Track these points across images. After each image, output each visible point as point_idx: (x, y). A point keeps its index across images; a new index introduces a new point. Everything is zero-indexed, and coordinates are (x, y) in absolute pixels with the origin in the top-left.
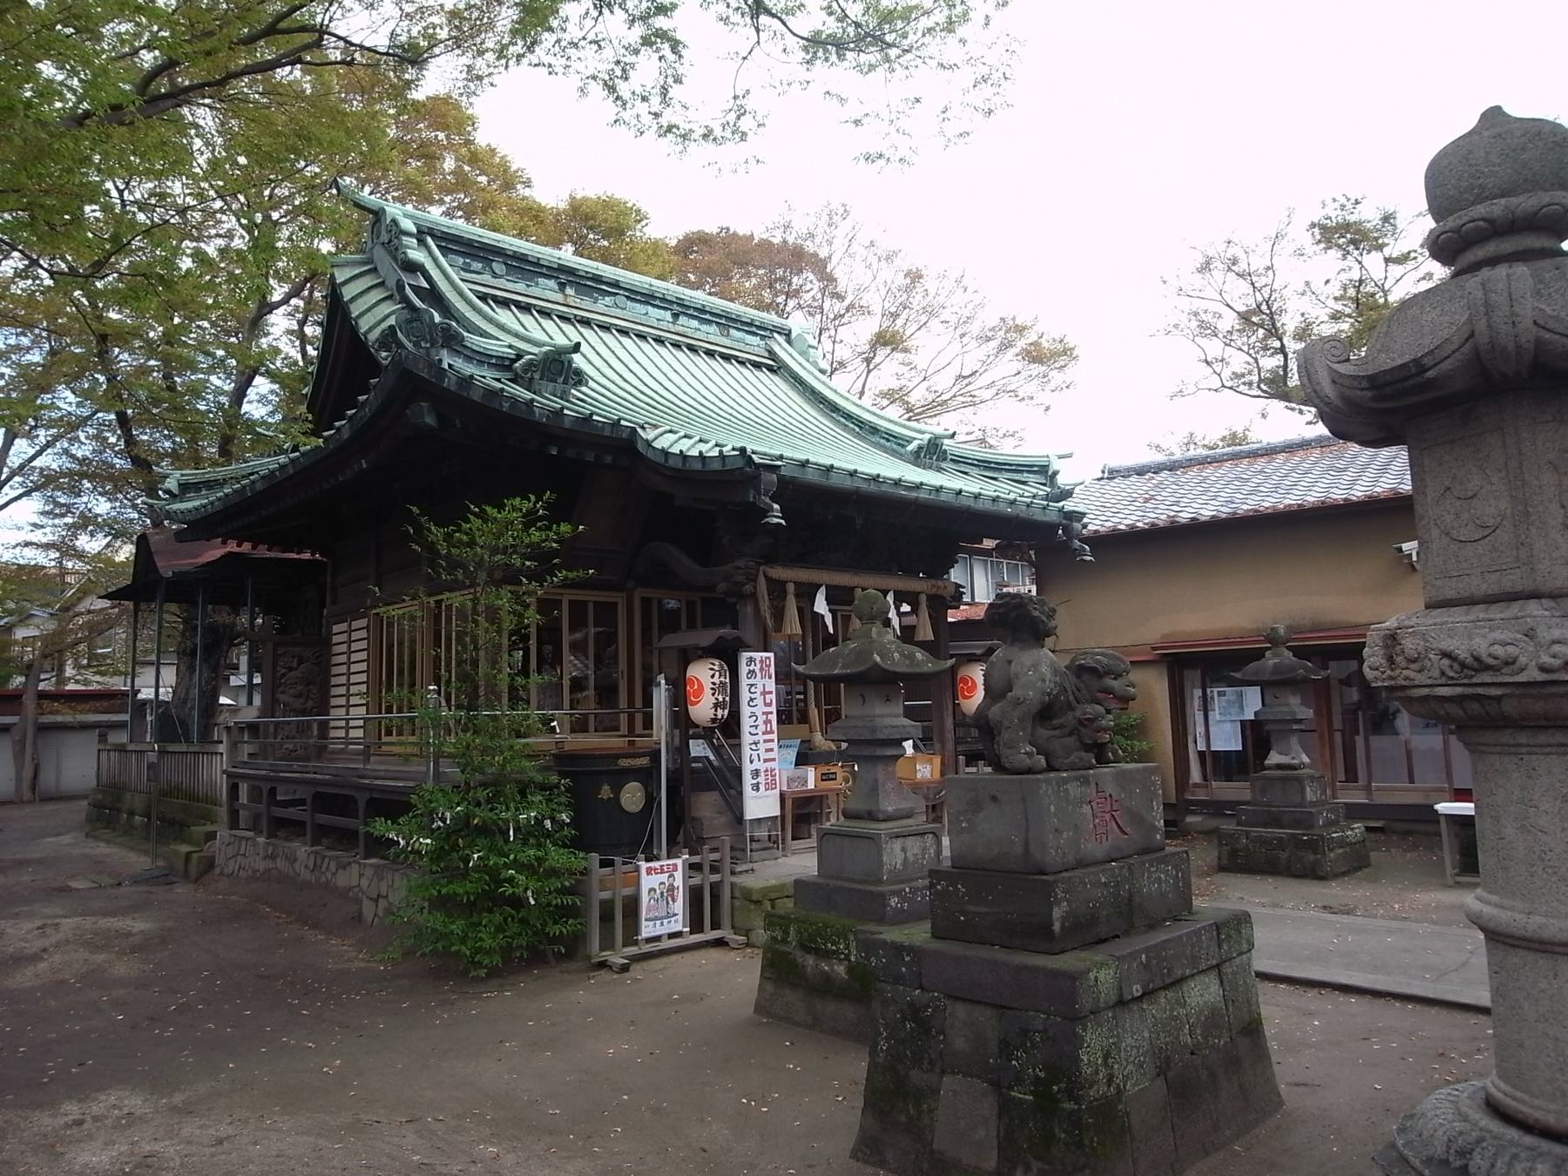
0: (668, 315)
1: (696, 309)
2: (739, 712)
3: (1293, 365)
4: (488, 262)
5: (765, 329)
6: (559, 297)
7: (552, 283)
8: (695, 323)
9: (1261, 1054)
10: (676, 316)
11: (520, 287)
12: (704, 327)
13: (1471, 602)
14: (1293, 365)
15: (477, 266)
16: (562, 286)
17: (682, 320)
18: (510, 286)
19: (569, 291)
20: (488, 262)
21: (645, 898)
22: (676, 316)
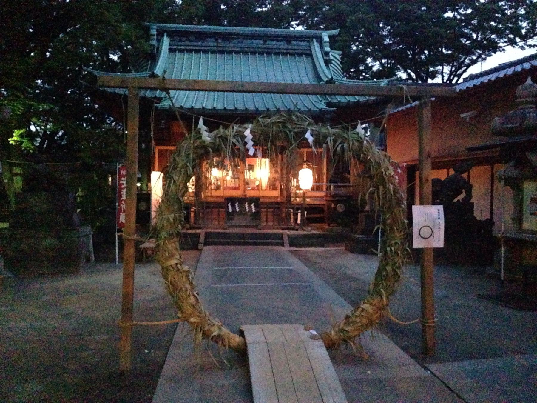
0: (262, 42)
5: (309, 38)
7: (212, 39)
10: (265, 41)
12: (278, 43)
15: (184, 39)
22: (265, 41)
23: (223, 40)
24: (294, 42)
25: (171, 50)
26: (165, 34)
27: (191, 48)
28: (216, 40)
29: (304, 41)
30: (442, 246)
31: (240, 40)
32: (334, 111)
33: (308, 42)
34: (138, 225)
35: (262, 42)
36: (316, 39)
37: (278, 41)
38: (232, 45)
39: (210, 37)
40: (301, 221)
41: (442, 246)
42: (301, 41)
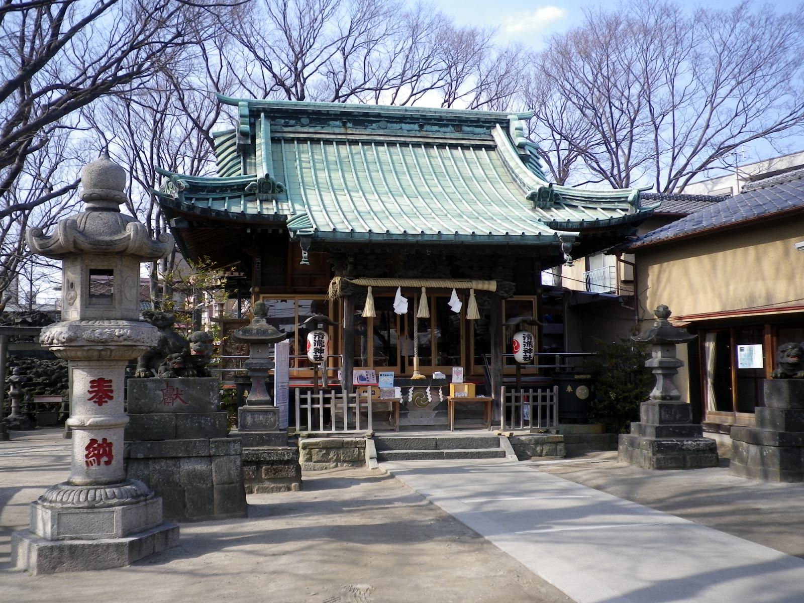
0: (416, 127)
1: (436, 119)
2: (396, 460)
3: (504, 322)
4: (298, 119)
5: (489, 122)
6: (342, 130)
7: (338, 123)
8: (436, 128)
9: (96, 569)
10: (421, 127)
11: (318, 129)
12: (443, 129)
13: (452, 486)
14: (504, 322)
15: (292, 122)
16: (344, 124)
17: (427, 127)
18: (311, 130)
19: (349, 125)
20: (298, 119)
21: (127, 552)
22: (421, 127)
23: (354, 125)
24: (466, 129)
25: (275, 141)
26: (262, 115)
27: (292, 135)
28: (344, 124)
29: (483, 127)
30: (543, 283)
31: (381, 124)
32: (576, 237)
33: (488, 128)
34: (660, 456)
35: (416, 127)
36: (500, 123)
37: (441, 126)
38: (368, 131)
39: (336, 120)
40: (490, 278)
41: (543, 283)
42: (476, 127)
